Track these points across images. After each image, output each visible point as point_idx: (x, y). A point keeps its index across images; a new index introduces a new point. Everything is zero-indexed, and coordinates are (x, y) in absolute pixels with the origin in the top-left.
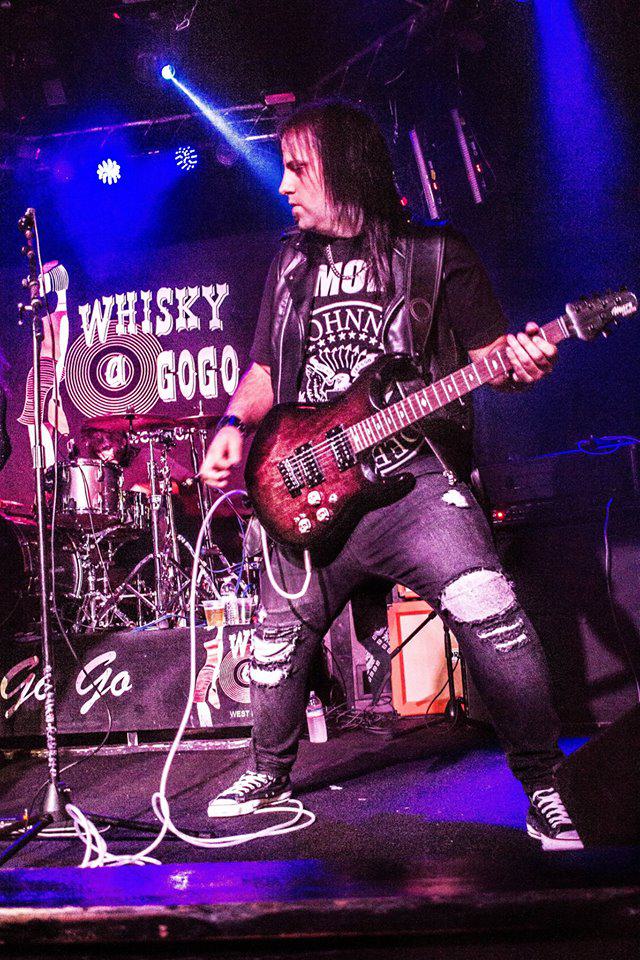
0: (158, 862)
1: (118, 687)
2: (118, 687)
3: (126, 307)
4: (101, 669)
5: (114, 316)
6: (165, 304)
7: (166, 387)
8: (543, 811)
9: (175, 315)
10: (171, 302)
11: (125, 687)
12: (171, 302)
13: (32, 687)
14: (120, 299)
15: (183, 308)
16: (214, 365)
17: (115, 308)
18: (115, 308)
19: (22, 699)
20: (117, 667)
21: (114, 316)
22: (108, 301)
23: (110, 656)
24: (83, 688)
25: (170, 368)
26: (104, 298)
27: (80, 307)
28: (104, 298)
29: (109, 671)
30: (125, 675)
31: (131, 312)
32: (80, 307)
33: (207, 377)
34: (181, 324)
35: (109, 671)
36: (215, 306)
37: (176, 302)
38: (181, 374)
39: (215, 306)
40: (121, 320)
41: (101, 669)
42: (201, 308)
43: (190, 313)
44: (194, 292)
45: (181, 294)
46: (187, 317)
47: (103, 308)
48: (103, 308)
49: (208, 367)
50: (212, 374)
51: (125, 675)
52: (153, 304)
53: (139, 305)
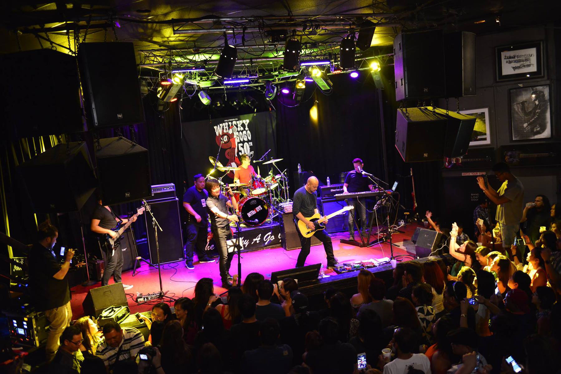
0: (273, 295)
1: (272, 239)
2: (272, 239)
3: (226, 126)
4: (268, 236)
5: (223, 129)
6: (235, 125)
8: (52, 136)
11: (273, 238)
13: (270, 238)
14: (224, 124)
15: (239, 126)
17: (223, 126)
18: (223, 126)
19: (268, 240)
20: (271, 235)
21: (223, 129)
22: (221, 125)
23: (270, 233)
24: (265, 239)
26: (220, 124)
27: (214, 127)
28: (220, 124)
29: (270, 236)
30: (273, 236)
31: (227, 127)
32: (214, 127)
35: (270, 236)
36: (246, 125)
37: (237, 124)
39: (246, 125)
40: (225, 129)
41: (268, 236)
42: (243, 125)
43: (241, 127)
45: (238, 122)
46: (240, 127)
47: (220, 126)
48: (220, 126)
49: (245, 135)
51: (273, 236)
52: (232, 125)
53: (229, 125)
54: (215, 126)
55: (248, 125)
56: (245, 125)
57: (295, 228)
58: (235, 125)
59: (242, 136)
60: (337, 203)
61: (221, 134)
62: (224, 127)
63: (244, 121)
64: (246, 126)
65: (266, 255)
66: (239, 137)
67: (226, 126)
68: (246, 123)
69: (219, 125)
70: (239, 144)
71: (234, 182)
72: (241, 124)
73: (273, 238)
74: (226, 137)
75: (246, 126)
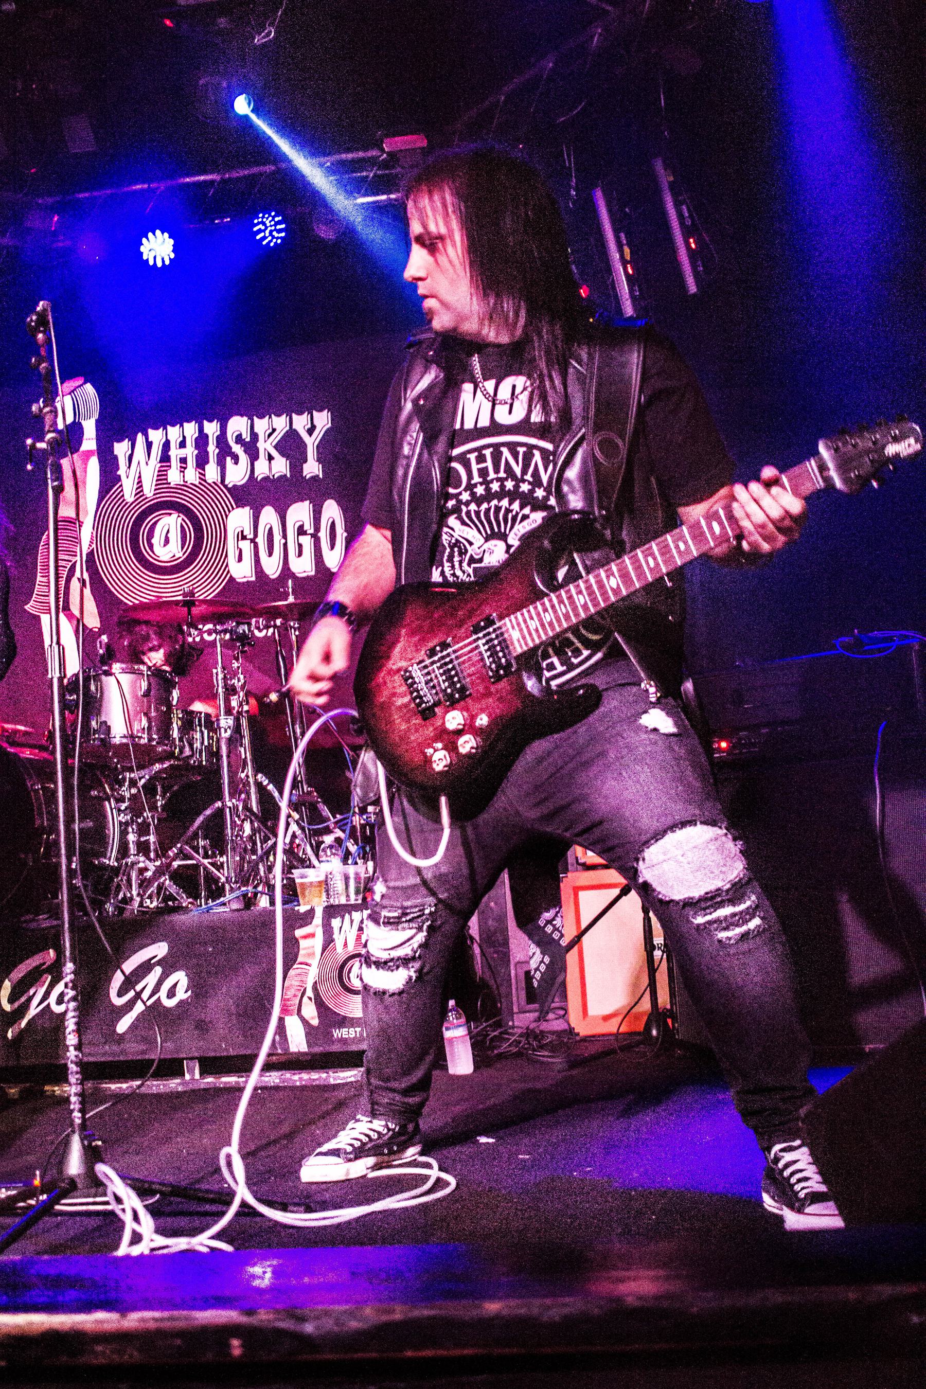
1: (171, 993)
2: (171, 993)
3: (183, 444)
4: (145, 968)
5: (165, 458)
6: (239, 439)
7: (240, 559)
9: (253, 455)
10: (247, 437)
12: (247, 437)
14: (174, 433)
15: (265, 446)
16: (309, 528)
17: (167, 445)
18: (167, 445)
20: (169, 965)
21: (165, 458)
22: (156, 436)
23: (160, 949)
24: (120, 995)
25: (306, 527)
29: (158, 970)
30: (180, 978)
33: (300, 546)
34: (262, 469)
35: (158, 970)
36: (311, 443)
37: (254, 436)
38: (261, 540)
39: (311, 443)
40: (174, 462)
41: (145, 968)
43: (274, 453)
44: (280, 423)
45: (261, 425)
46: (270, 458)
47: (149, 445)
48: (149, 445)
49: (301, 531)
50: (306, 541)
51: (180, 978)
53: (202, 441)
54: (120, 440)
55: (321, 447)
56: (305, 446)
57: (624, 897)
58: (239, 439)
59: (277, 537)
60: (547, 1021)
61: (149, 490)
62: (175, 453)
63: (300, 422)
64: (311, 453)
65: (877, 969)
66: (253, 541)
67: (183, 444)
68: (310, 431)
69: (146, 436)
70: (336, 923)
71: (271, 908)
72: (276, 437)
73: (182, 994)
74: (171, 523)
75: (311, 453)
